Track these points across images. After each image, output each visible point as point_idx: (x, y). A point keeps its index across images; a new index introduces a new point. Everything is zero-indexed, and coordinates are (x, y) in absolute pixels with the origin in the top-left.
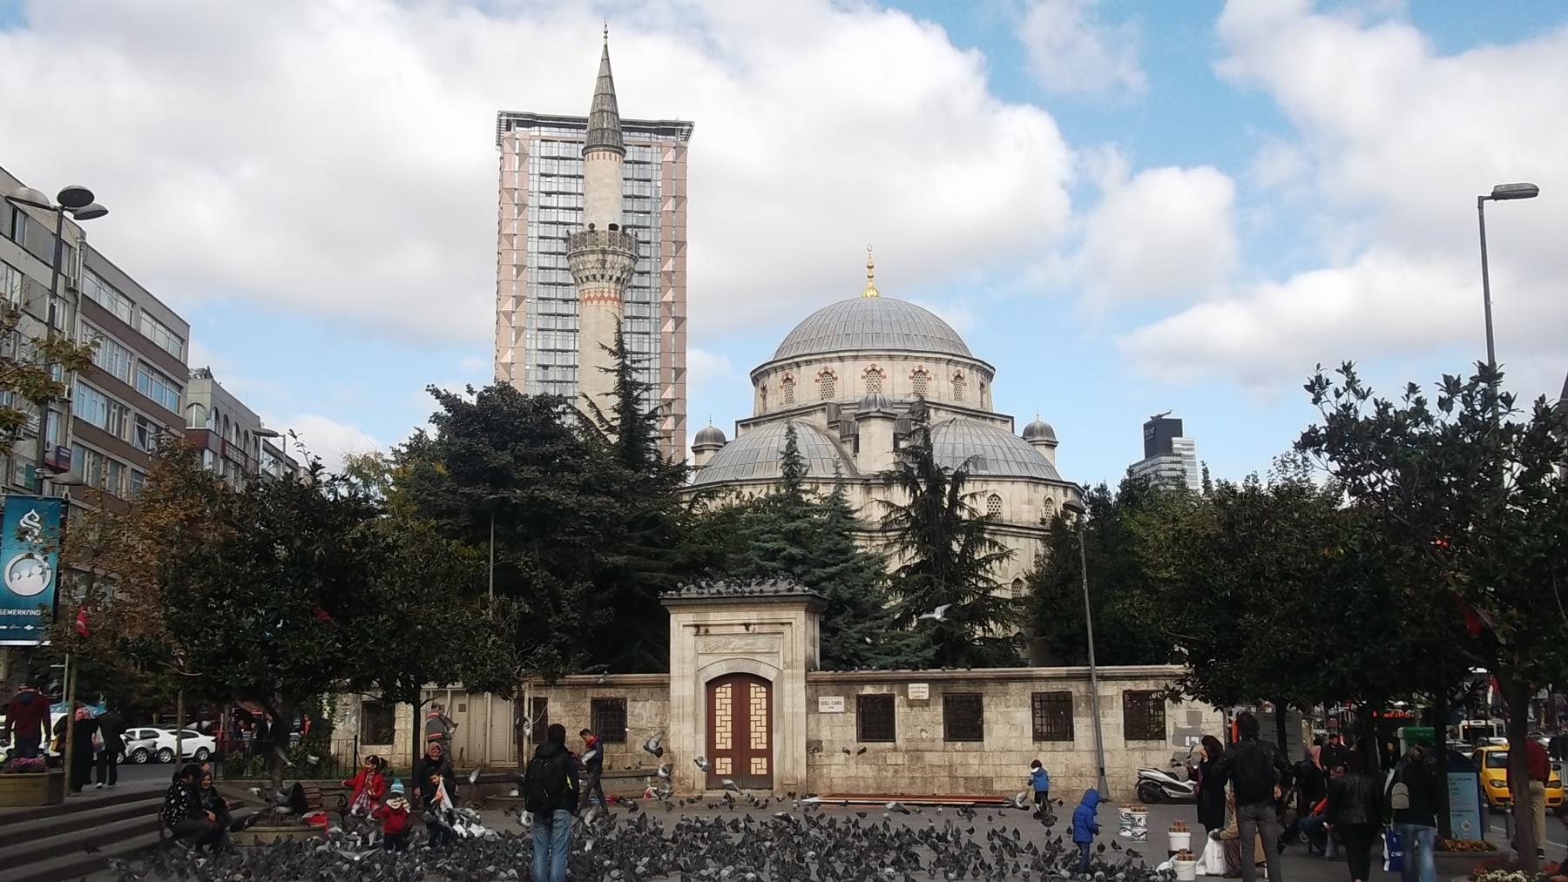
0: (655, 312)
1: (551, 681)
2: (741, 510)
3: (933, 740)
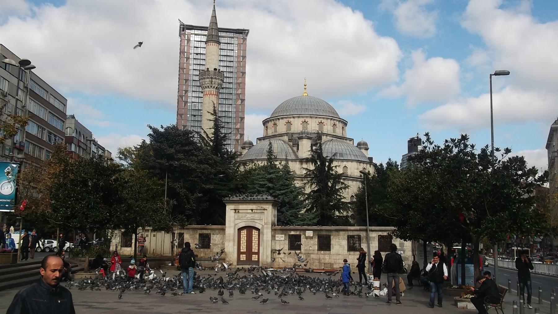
0: (234, 97)
1: (183, 227)
2: (255, 170)
3: (314, 250)
